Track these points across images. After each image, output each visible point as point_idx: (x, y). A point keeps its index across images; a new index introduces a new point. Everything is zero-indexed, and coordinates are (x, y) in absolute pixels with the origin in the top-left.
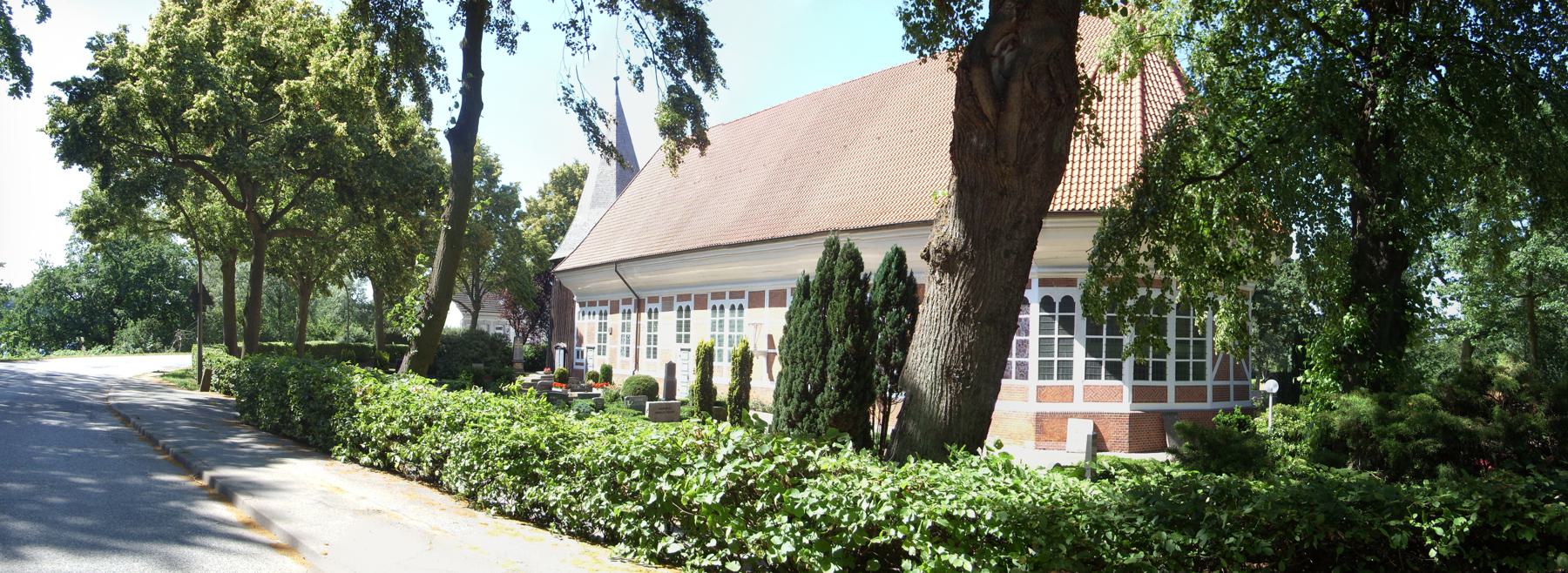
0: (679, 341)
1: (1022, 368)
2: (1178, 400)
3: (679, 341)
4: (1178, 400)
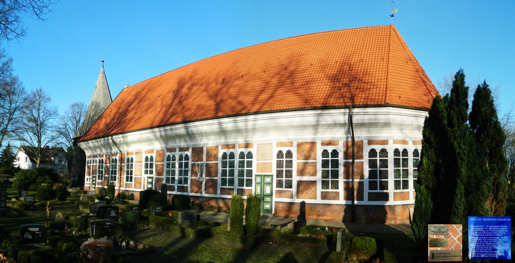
0: (146, 172)
1: (280, 182)
2: (370, 199)
3: (146, 172)
4: (370, 199)
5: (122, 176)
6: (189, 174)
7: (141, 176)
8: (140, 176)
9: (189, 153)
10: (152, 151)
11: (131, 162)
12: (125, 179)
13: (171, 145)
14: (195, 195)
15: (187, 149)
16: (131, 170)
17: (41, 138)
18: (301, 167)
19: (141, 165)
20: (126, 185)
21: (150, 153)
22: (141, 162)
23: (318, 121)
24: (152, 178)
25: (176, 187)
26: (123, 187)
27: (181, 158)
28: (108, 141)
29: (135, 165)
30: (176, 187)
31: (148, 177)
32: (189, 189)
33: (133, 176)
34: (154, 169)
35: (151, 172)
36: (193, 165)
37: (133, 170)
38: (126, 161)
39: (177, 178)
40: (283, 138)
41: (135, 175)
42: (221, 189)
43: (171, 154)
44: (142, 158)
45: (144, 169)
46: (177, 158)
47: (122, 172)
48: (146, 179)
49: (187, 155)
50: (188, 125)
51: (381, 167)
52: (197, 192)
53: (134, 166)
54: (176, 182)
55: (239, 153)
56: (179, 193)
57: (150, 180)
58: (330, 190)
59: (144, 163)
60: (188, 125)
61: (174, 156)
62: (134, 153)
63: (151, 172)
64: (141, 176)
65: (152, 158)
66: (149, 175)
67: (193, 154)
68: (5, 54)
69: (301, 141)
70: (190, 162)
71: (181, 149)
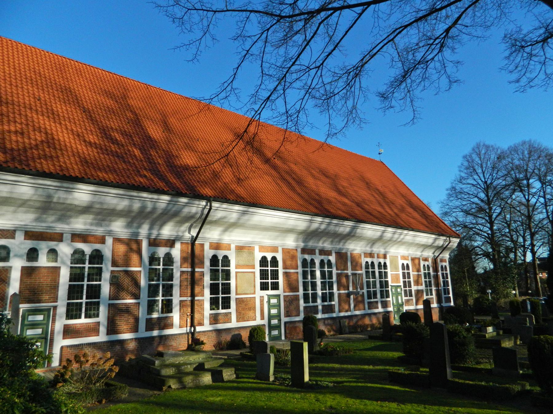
0: (264, 287)
3: (264, 287)
5: (196, 298)
6: (335, 287)
7: (254, 293)
8: (253, 294)
9: (333, 258)
10: (275, 249)
11: (384, 269)
12: (207, 305)
13: (311, 244)
14: (347, 314)
15: (329, 253)
16: (405, 279)
17: (329, 212)
18: (416, 278)
19: (254, 273)
20: (215, 319)
21: (273, 252)
22: (253, 267)
23: (239, 219)
24: (278, 296)
25: (320, 308)
26: (201, 324)
27: (322, 263)
28: (182, 209)
29: (236, 273)
30: (320, 308)
31: (270, 297)
32: (337, 309)
33: (233, 296)
34: (281, 280)
35: (275, 286)
36: (338, 275)
37: (233, 282)
38: (207, 263)
39: (319, 292)
40: (268, 240)
41: (237, 294)
42: (369, 303)
43: (308, 257)
44: (253, 259)
45: (258, 281)
46: (317, 262)
47: (197, 290)
48: (266, 299)
49: (329, 261)
50: (358, 225)
51: (158, 286)
52: (347, 311)
53: (233, 275)
54: (319, 301)
55: (210, 256)
56: (326, 316)
57: (274, 301)
58: (221, 311)
59: (257, 269)
60: (358, 225)
61: (312, 260)
62: (233, 247)
63: (275, 286)
64: (254, 293)
65: (97, 257)
66: (271, 292)
67: (170, 256)
68: (385, 86)
69: (413, 256)
70: (335, 271)
71: (323, 252)
